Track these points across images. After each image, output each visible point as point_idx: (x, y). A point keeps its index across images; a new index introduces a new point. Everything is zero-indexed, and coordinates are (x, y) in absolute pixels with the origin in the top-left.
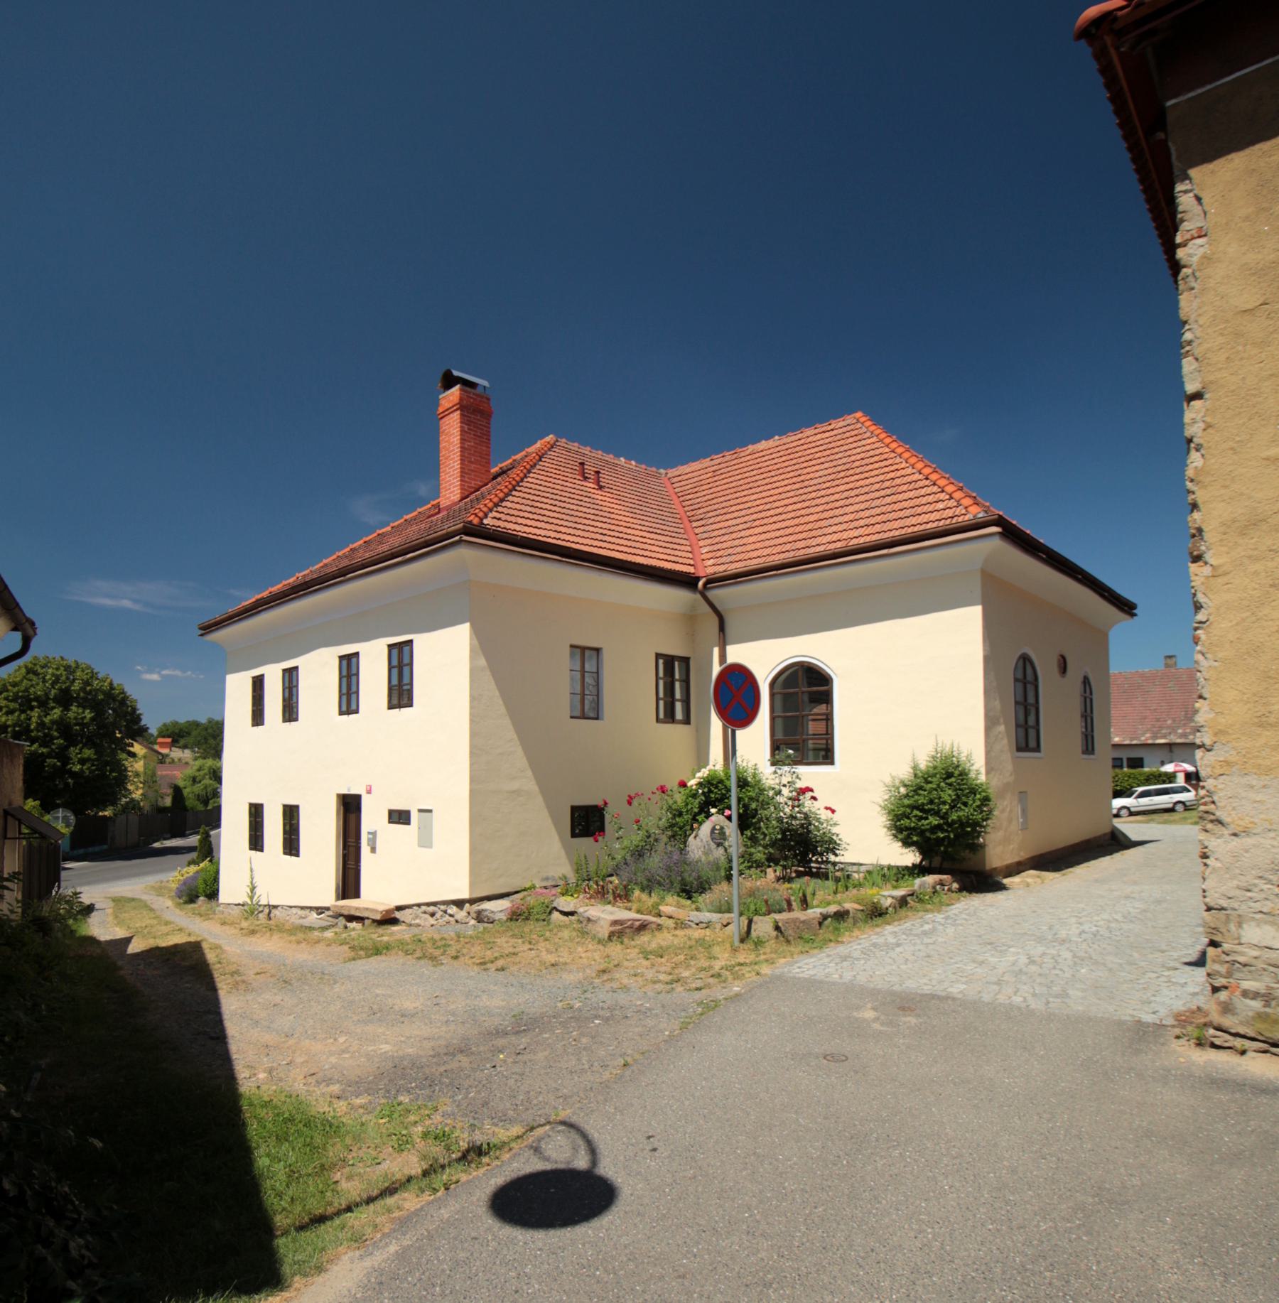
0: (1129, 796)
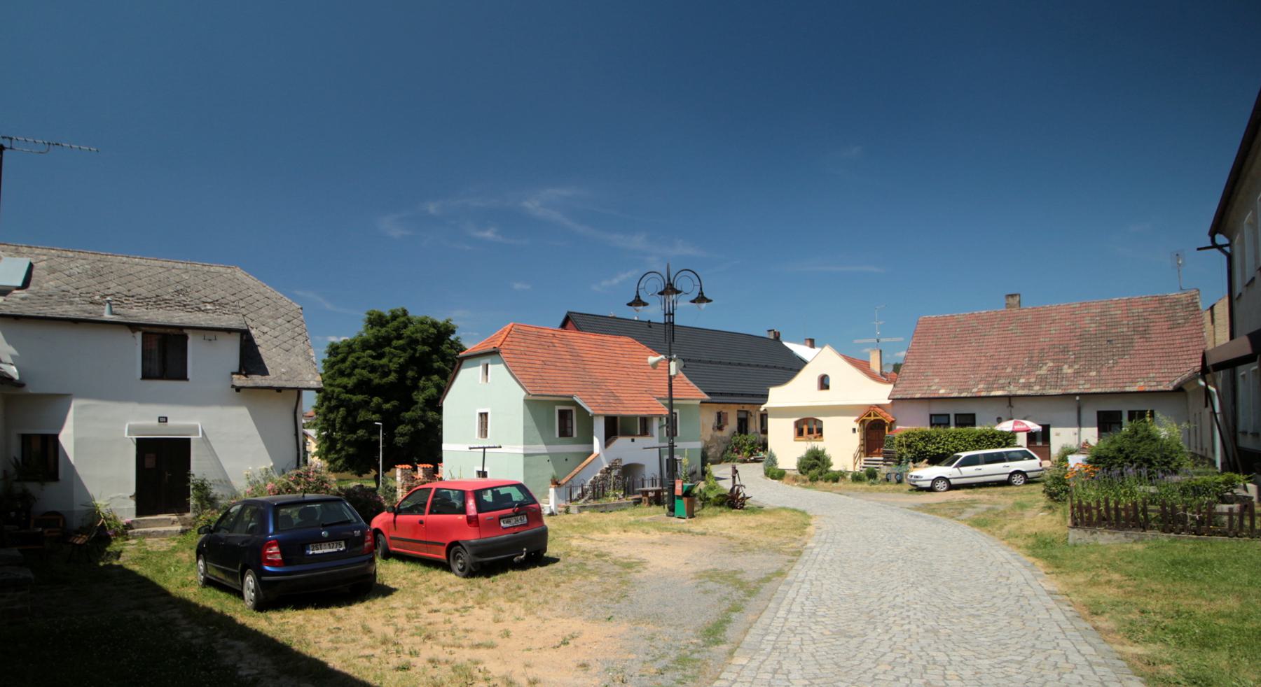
0: (950, 464)
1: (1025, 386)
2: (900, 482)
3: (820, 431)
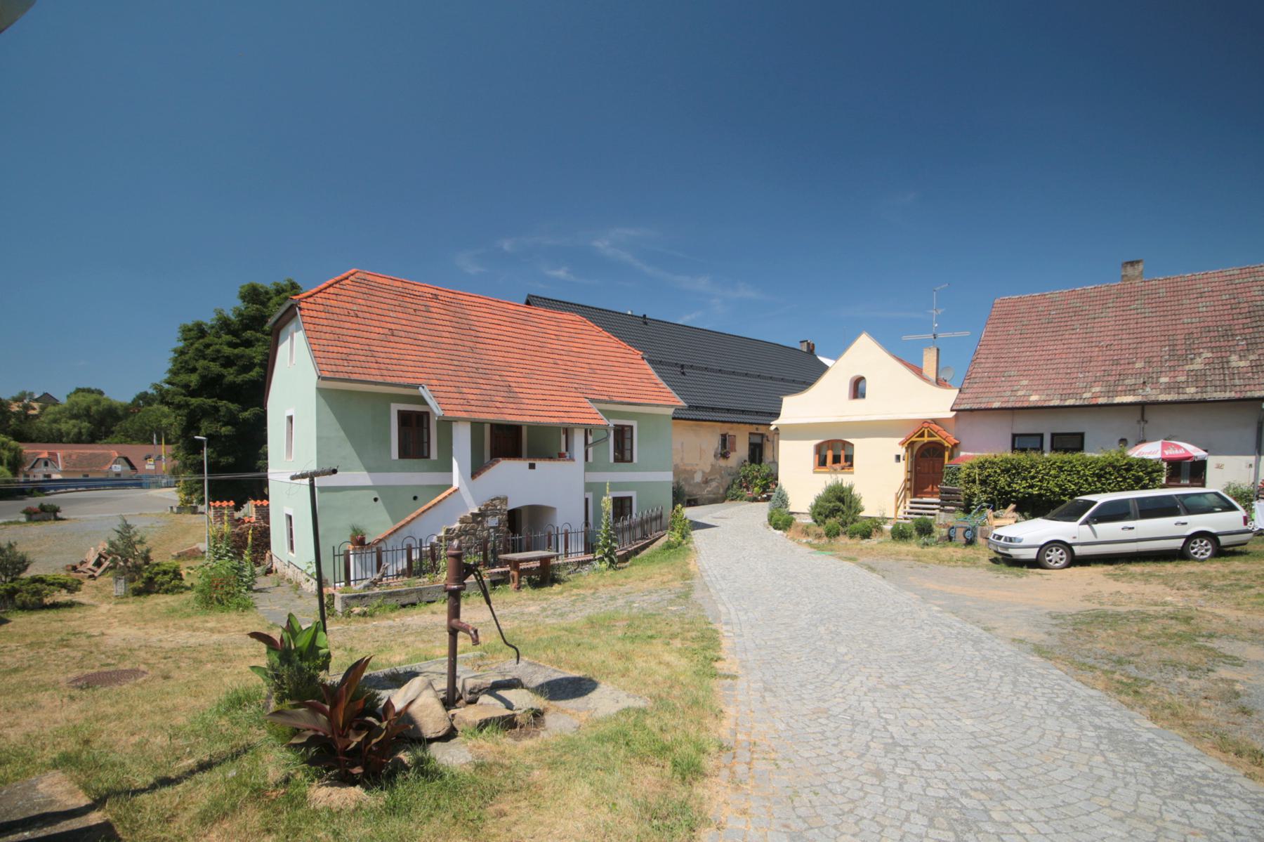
1: (1169, 388)
2: (970, 542)
3: (849, 459)
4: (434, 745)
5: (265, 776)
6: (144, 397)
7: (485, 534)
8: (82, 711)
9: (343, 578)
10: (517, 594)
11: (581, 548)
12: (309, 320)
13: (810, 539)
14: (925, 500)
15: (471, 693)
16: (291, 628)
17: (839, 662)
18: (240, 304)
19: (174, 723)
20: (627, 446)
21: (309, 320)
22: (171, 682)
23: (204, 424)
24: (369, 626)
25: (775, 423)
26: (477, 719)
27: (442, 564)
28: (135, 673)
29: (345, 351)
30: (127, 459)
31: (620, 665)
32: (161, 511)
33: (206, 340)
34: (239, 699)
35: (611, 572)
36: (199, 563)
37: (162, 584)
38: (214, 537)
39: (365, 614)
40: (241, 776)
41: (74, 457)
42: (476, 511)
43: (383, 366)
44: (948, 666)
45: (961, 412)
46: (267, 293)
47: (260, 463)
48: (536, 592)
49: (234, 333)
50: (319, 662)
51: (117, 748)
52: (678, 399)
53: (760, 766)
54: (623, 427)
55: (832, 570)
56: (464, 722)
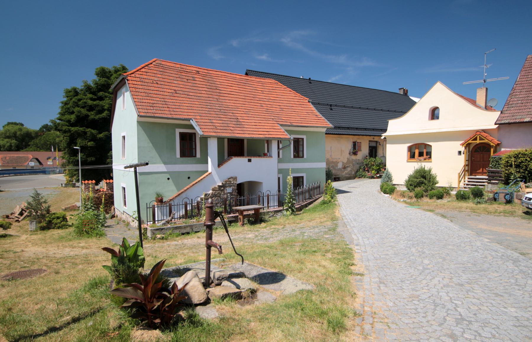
3: (429, 154)
4: (198, 307)
5: (108, 325)
6: (46, 127)
7: (225, 196)
8: (8, 293)
9: (152, 219)
10: (242, 228)
11: (276, 203)
12: (132, 86)
13: (405, 199)
14: (477, 177)
15: (218, 280)
16: (124, 245)
17: (425, 269)
18: (96, 78)
19: (60, 297)
20: (301, 149)
21: (132, 86)
22: (60, 275)
23: (79, 141)
24: (165, 244)
25: (384, 135)
26: (221, 294)
27: (203, 212)
28: (40, 271)
29: (151, 102)
30: (37, 159)
31: (298, 266)
32: (57, 186)
33: (79, 97)
34: (96, 283)
35: (292, 216)
36: (76, 213)
37: (56, 224)
38: (85, 199)
39: (163, 238)
40: (95, 325)
41: (8, 158)
42: (221, 184)
43: (171, 109)
44: (496, 274)
45: (501, 125)
46: (110, 72)
47: (108, 160)
48: (252, 227)
49: (94, 93)
50: (139, 263)
51: (27, 312)
52: (328, 123)
53: (378, 326)
54: (298, 139)
55: (420, 217)
56: (214, 295)
